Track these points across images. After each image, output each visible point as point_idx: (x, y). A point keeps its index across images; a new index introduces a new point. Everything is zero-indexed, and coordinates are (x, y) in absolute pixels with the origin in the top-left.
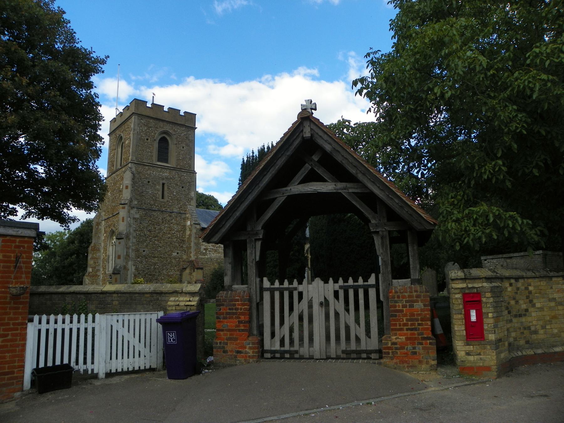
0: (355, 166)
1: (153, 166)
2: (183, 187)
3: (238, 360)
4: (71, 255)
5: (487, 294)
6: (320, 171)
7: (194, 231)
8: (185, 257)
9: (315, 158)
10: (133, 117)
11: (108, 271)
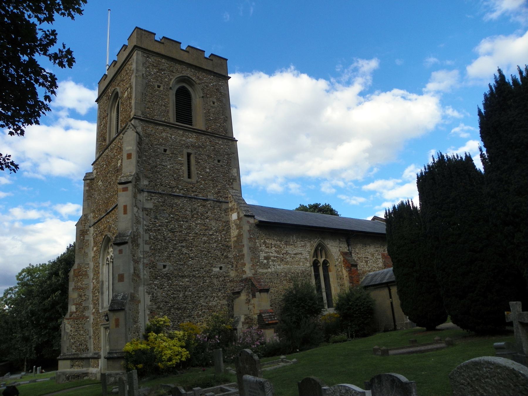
2: (219, 161)
4: (54, 291)
7: (246, 228)
8: (233, 274)
10: (135, 56)
11: (102, 308)
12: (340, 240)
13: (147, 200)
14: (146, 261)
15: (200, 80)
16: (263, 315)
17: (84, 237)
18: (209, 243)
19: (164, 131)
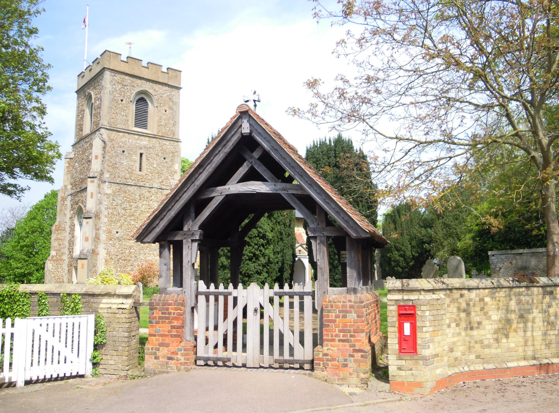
0: (292, 167)
2: (165, 159)
3: (170, 367)
5: (422, 307)
6: (261, 169)
9: (256, 154)
14: (104, 228)
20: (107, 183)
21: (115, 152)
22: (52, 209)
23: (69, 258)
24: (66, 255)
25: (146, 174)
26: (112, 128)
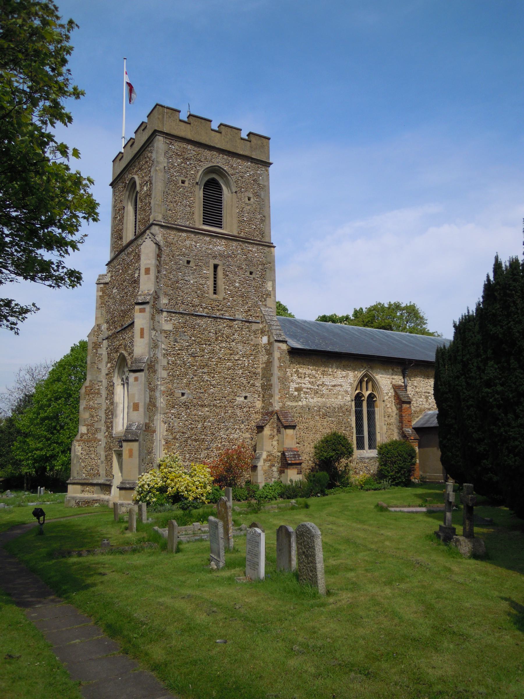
1: (196, 232)
2: (251, 273)
12: (393, 370)
13: (165, 320)
14: (163, 388)
15: (234, 169)
16: (287, 454)
17: (97, 350)
18: (234, 369)
19: (188, 238)
20: (165, 314)
21: (176, 263)
22: (81, 366)
23: (106, 437)
24: (102, 433)
25: (224, 299)
26: (169, 225)
